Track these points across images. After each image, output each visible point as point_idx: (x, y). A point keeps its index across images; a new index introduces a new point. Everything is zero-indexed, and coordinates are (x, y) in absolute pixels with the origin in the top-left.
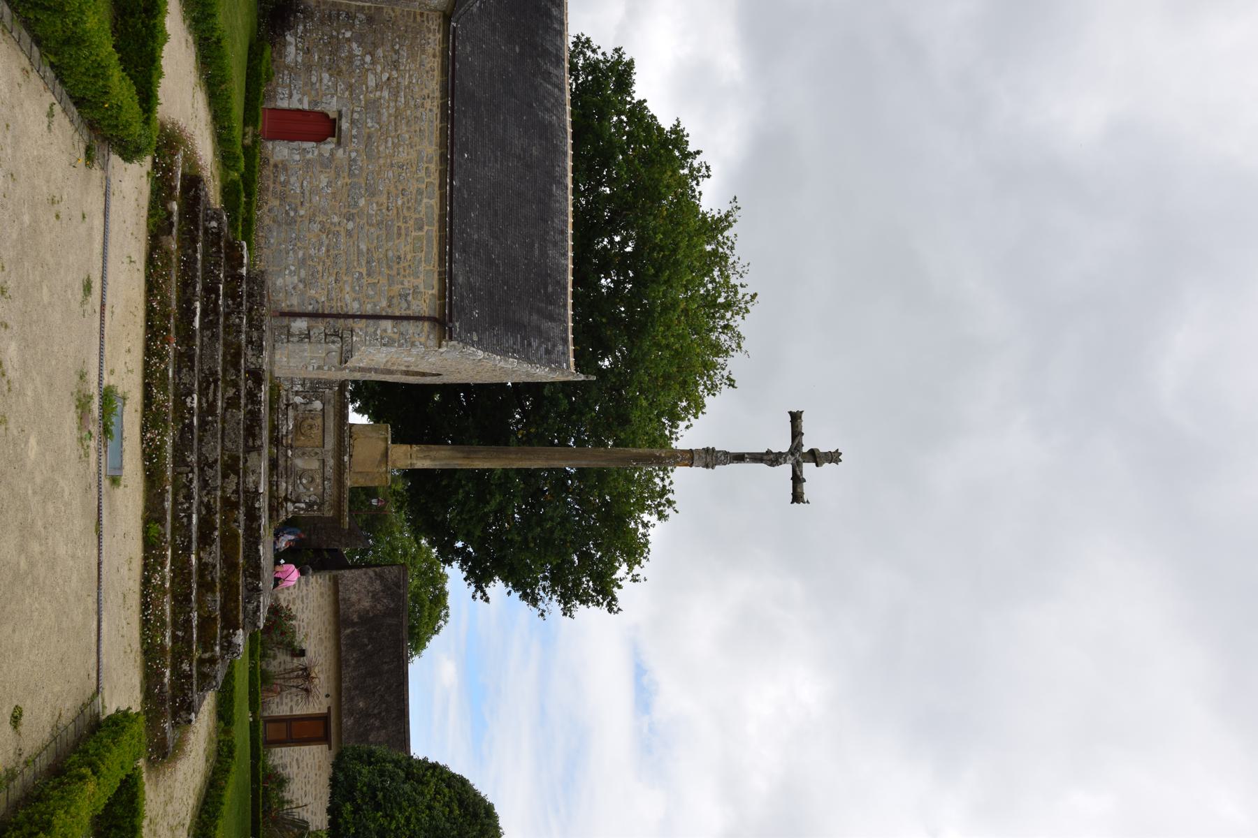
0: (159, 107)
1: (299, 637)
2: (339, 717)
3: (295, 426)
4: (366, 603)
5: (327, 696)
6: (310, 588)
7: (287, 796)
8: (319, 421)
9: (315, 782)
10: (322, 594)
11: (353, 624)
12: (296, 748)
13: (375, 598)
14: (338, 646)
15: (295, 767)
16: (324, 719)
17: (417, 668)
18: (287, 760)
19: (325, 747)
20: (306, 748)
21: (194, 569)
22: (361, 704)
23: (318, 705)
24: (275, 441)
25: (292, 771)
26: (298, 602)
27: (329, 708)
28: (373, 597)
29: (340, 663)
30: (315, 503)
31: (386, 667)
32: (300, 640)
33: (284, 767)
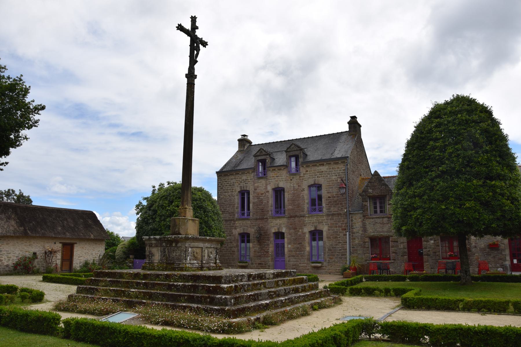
0: (512, 326)
1: (28, 254)
2: (65, 239)
3: (195, 260)
4: (13, 222)
5: (55, 243)
6: (3, 250)
7: (91, 262)
8: (194, 249)
9: (88, 250)
10: (7, 244)
11: (25, 230)
12: (74, 257)
13: (9, 218)
14: (34, 238)
15: (81, 258)
16: (64, 245)
17: (35, 203)
18: (78, 261)
19: (75, 245)
20: (75, 253)
21: (271, 300)
22: (60, 229)
23: (58, 246)
24: (201, 268)
25: (83, 260)
26: (10, 255)
27: (60, 243)
28: (9, 219)
29: (44, 237)
30: (216, 251)
31: (41, 216)
32: (29, 255)
33: (80, 263)
